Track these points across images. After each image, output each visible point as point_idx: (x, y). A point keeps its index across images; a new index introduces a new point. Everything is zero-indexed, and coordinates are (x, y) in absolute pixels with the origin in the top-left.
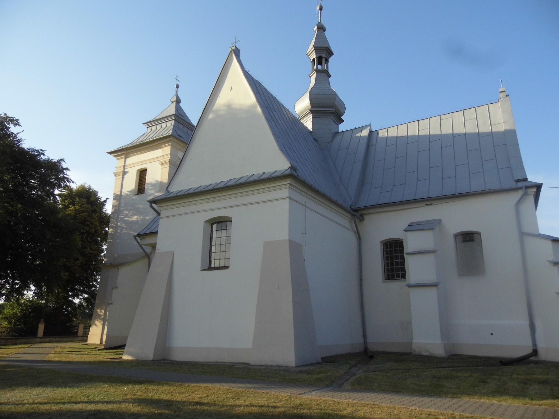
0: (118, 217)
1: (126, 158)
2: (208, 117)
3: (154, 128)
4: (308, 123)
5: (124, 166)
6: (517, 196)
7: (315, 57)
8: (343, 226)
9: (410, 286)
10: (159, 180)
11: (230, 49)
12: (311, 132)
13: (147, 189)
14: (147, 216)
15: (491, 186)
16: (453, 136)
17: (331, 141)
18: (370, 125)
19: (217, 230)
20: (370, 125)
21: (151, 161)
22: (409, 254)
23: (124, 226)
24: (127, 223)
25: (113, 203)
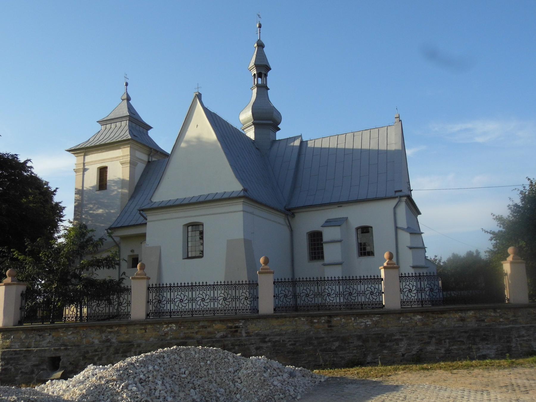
0: (82, 210)
1: (85, 156)
2: (181, 144)
3: (108, 126)
4: (251, 134)
5: (84, 164)
6: (394, 202)
7: (255, 72)
8: (279, 223)
9: (325, 265)
10: (121, 177)
11: (195, 94)
12: (253, 142)
13: (110, 185)
14: (112, 209)
15: (380, 195)
16: (361, 150)
17: (270, 149)
18: (301, 136)
19: (192, 231)
20: (301, 136)
21: (111, 160)
22: (327, 242)
23: (89, 218)
24: (92, 215)
25: (76, 197)
